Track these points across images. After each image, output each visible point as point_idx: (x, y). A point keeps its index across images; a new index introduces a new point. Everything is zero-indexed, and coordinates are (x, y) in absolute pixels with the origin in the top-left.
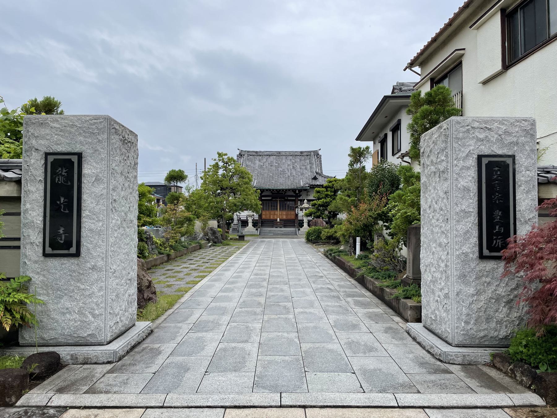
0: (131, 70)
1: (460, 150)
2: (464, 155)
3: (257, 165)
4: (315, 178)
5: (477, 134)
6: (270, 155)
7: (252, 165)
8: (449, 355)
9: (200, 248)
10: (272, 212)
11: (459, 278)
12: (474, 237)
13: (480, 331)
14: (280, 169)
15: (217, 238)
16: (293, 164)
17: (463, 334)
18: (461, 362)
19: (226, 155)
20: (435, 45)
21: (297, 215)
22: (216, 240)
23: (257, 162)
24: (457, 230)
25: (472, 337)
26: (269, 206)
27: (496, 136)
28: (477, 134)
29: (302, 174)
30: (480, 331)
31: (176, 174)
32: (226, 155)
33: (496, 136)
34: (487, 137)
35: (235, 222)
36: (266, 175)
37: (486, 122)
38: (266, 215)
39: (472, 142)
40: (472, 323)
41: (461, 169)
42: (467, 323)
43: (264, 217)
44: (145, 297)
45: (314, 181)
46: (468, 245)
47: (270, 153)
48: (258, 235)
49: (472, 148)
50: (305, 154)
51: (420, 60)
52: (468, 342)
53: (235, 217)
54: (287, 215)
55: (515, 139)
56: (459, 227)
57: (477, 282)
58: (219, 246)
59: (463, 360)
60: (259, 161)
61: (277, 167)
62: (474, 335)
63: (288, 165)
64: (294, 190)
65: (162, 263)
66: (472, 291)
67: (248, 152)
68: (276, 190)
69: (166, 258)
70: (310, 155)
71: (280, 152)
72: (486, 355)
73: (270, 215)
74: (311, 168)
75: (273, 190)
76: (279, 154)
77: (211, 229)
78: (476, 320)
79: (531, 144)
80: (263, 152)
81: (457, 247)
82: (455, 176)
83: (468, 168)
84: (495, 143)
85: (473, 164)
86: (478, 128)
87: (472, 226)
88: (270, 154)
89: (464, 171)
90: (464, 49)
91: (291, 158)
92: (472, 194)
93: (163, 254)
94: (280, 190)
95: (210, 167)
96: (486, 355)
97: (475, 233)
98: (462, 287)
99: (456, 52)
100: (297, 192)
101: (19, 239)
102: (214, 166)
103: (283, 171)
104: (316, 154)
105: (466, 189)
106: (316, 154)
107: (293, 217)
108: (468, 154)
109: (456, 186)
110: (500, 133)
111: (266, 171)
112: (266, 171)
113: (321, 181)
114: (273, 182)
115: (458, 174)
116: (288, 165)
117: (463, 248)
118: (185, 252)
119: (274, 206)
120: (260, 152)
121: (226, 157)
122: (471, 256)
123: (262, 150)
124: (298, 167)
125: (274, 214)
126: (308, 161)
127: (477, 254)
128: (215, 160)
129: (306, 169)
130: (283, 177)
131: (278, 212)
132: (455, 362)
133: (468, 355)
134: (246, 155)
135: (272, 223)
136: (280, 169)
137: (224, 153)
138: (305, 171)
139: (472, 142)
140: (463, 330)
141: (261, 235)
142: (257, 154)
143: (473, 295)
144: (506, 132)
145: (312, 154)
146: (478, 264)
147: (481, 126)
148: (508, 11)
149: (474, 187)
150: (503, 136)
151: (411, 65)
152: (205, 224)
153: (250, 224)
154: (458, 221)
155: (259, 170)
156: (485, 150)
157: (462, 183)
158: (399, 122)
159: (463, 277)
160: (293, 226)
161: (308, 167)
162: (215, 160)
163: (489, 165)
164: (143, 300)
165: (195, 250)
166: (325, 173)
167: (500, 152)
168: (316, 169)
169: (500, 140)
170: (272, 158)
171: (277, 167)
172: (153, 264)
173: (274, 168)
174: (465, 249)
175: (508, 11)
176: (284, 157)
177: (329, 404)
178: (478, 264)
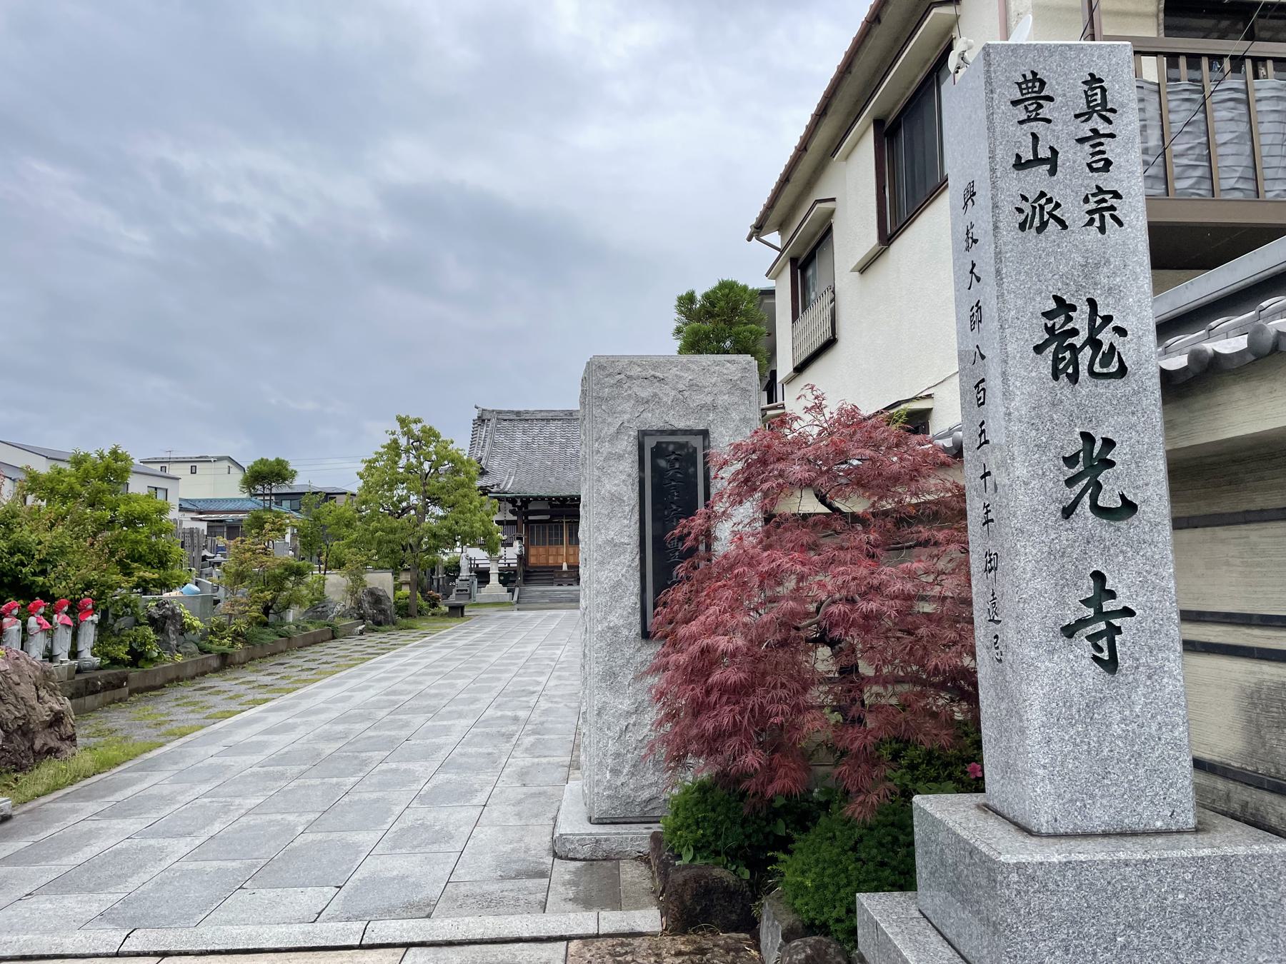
0: (234, 227)
1: (604, 421)
2: (613, 430)
3: (518, 443)
5: (636, 389)
7: (507, 443)
8: (568, 840)
9: (334, 638)
10: (553, 550)
11: (603, 679)
12: (632, 594)
13: (643, 787)
15: (382, 611)
17: (609, 796)
18: (588, 856)
19: (417, 421)
20: (791, 190)
22: (381, 617)
23: (519, 435)
24: (599, 582)
25: (629, 803)
26: (544, 536)
27: (673, 393)
28: (636, 389)
30: (643, 787)
31: (265, 469)
32: (417, 421)
33: (673, 393)
34: (655, 395)
35: (464, 573)
37: (655, 367)
38: (537, 556)
39: (627, 406)
40: (625, 771)
41: (606, 459)
42: (616, 772)
43: (532, 560)
44: (38, 745)
46: (619, 611)
48: (511, 604)
49: (626, 417)
51: (775, 216)
52: (619, 813)
55: (709, 399)
56: (603, 575)
57: (638, 686)
58: (383, 632)
59: (594, 851)
60: (524, 432)
61: (563, 447)
62: (629, 797)
65: (203, 674)
66: (626, 704)
67: (499, 412)
68: (557, 498)
69: (215, 663)
72: (642, 839)
75: (550, 498)
77: (372, 593)
78: (634, 766)
79: (742, 408)
80: (534, 412)
81: (599, 615)
82: (596, 472)
83: (620, 457)
84: (672, 407)
85: (629, 449)
86: (638, 377)
87: (627, 571)
89: (611, 463)
90: (833, 200)
92: (627, 509)
93: (209, 652)
94: (565, 498)
95: (382, 450)
96: (642, 839)
97: (634, 586)
98: (609, 697)
99: (818, 205)
100: (519, 504)
101: (1190, 647)
102: (388, 447)
105: (616, 499)
108: (619, 429)
109: (598, 492)
110: (681, 387)
111: (538, 455)
112: (538, 455)
114: (552, 479)
115: (601, 469)
117: (610, 618)
118: (283, 647)
119: (557, 535)
120: (527, 412)
121: (419, 425)
122: (625, 632)
127: (638, 629)
128: (393, 434)
132: (578, 856)
133: (606, 840)
137: (412, 417)
139: (627, 406)
140: (609, 788)
141: (521, 604)
142: (520, 417)
143: (629, 714)
144: (692, 386)
146: (639, 650)
147: (644, 374)
148: (887, 125)
149: (631, 496)
150: (686, 394)
151: (759, 229)
152: (357, 578)
153: (494, 579)
154: (602, 563)
155: (523, 454)
156: (654, 420)
157: (608, 487)
159: (610, 676)
162: (393, 434)
163: (658, 451)
164: (30, 753)
165: (315, 640)
167: (681, 424)
169: (680, 401)
170: (553, 425)
171: (563, 447)
172: (172, 675)
173: (556, 449)
174: (614, 619)
175: (887, 125)
177: (217, 948)
178: (639, 650)
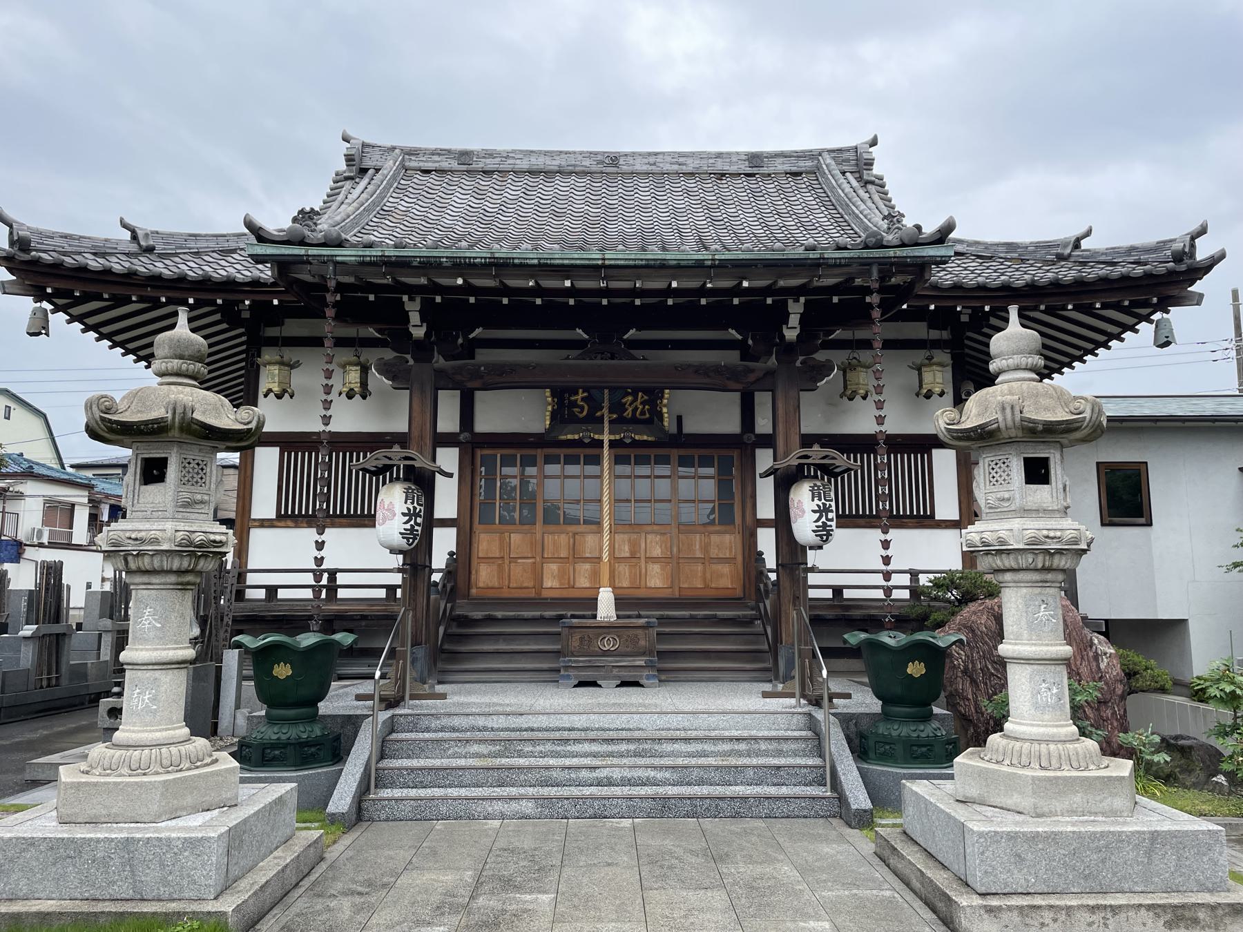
50: (781, 166)
54: (674, 562)
60: (479, 194)
70: (815, 172)
71: (614, 159)
107: (726, 579)
120: (490, 154)
125: (576, 557)
135: (553, 639)
176: (644, 183)
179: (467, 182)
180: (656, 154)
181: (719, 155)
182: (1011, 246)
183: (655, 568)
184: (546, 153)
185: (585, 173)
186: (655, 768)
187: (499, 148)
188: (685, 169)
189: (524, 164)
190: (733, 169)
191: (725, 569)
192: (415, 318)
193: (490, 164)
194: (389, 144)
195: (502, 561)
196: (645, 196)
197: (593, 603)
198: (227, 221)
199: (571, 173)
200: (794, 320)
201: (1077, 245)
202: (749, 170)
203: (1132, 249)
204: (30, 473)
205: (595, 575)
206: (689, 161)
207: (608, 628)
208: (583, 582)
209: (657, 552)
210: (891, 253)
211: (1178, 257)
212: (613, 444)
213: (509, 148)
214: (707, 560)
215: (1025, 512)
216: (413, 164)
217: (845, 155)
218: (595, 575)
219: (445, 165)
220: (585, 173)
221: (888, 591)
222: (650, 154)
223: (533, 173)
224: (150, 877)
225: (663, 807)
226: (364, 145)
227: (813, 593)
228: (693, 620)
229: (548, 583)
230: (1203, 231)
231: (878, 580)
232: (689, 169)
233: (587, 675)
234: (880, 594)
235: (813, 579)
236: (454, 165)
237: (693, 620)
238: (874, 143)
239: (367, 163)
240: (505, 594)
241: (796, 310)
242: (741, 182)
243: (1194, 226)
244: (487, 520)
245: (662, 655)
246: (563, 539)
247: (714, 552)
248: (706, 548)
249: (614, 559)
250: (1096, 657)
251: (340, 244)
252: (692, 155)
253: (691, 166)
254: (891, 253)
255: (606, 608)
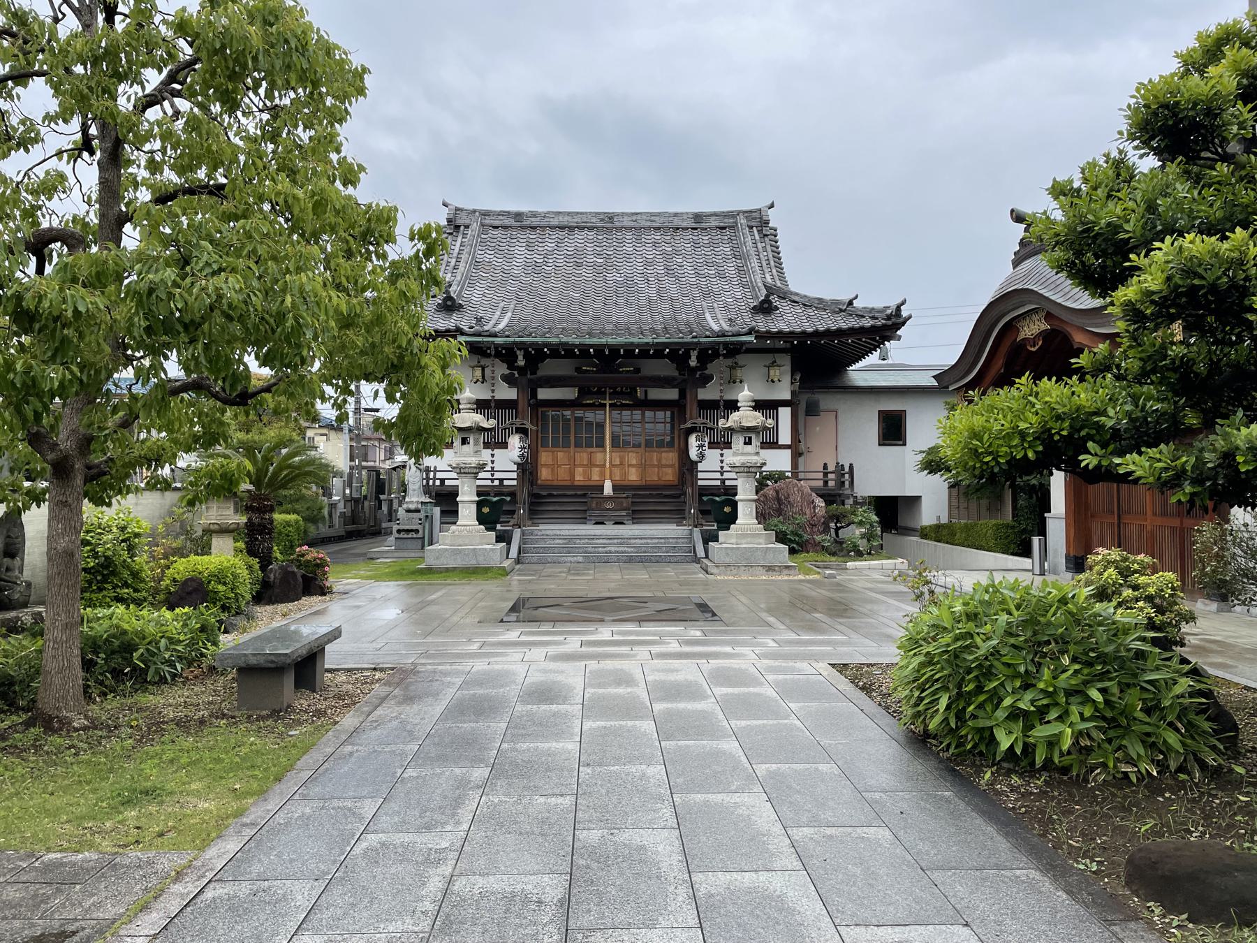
3: (518, 262)
4: (765, 308)
6: (571, 228)
7: (498, 262)
10: (582, 456)
14: (613, 276)
16: (667, 258)
21: (688, 468)
23: (520, 251)
29: (707, 294)
36: (553, 296)
38: (553, 467)
43: (544, 474)
45: (760, 318)
47: (573, 221)
50: (714, 222)
53: (413, 476)
54: (643, 467)
60: (529, 246)
61: (600, 271)
63: (647, 263)
64: (676, 353)
67: (485, 214)
70: (733, 227)
71: (611, 217)
73: (573, 465)
74: (741, 271)
76: (607, 224)
80: (545, 215)
88: (570, 226)
91: (657, 236)
100: (693, 362)
103: (628, 282)
104: (759, 223)
106: (759, 223)
107: (669, 475)
113: (788, 320)
116: (647, 263)
120: (534, 215)
123: (541, 209)
124: (688, 267)
125: (591, 464)
126: (727, 248)
129: (721, 275)
130: (629, 304)
131: (607, 456)
134: (475, 226)
135: (581, 502)
136: (613, 276)
138: (717, 285)
145: (742, 221)
158: (444, 717)
160: (678, 515)
161: (731, 269)
166: (800, 281)
168: (761, 277)
170: (579, 237)
171: (600, 271)
173: (587, 273)
176: (629, 235)
179: (523, 236)
180: (637, 214)
181: (676, 215)
182: (820, 300)
183: (633, 470)
184: (568, 214)
185: (593, 228)
186: (664, 671)
187: (540, 210)
188: (655, 225)
189: (555, 222)
190: (684, 224)
191: (669, 471)
192: (521, 357)
193: (535, 222)
194: (471, 208)
195: (553, 467)
196: (628, 248)
197: (601, 488)
198: (874, 732)
199: (584, 228)
200: (694, 358)
201: (850, 303)
202: (694, 225)
203: (873, 309)
204: (938, 533)
205: (602, 474)
206: (657, 219)
207: (609, 498)
208: (595, 477)
209: (634, 462)
210: (728, 339)
211: (889, 317)
212: (611, 405)
213: (545, 210)
214: (660, 466)
215: (743, 454)
216: (487, 222)
217: (754, 215)
218: (602, 474)
219: (507, 223)
220: (593, 228)
221: (826, 483)
222: (633, 214)
223: (562, 228)
224: (481, 559)
225: (630, 560)
226: (457, 209)
227: (700, 483)
228: (651, 496)
229: (577, 478)
230: (903, 303)
231: (718, 475)
232: (657, 225)
233: (599, 519)
234: (718, 483)
235: (700, 475)
236: (512, 222)
237: (651, 496)
238: (772, 206)
239: (459, 222)
240: (555, 483)
241: (694, 355)
242: (689, 235)
243: (899, 301)
244: (545, 445)
245: (634, 512)
246: (585, 455)
247: (664, 462)
248: (659, 460)
249: (612, 465)
250: (814, 508)
251: (495, 336)
252: (658, 214)
253: (658, 222)
254: (728, 339)
255: (608, 489)
